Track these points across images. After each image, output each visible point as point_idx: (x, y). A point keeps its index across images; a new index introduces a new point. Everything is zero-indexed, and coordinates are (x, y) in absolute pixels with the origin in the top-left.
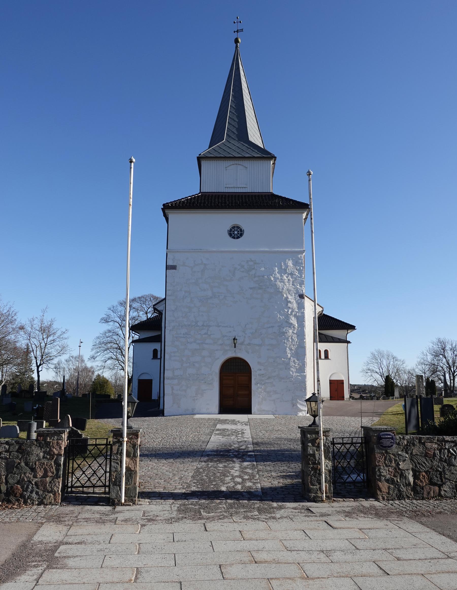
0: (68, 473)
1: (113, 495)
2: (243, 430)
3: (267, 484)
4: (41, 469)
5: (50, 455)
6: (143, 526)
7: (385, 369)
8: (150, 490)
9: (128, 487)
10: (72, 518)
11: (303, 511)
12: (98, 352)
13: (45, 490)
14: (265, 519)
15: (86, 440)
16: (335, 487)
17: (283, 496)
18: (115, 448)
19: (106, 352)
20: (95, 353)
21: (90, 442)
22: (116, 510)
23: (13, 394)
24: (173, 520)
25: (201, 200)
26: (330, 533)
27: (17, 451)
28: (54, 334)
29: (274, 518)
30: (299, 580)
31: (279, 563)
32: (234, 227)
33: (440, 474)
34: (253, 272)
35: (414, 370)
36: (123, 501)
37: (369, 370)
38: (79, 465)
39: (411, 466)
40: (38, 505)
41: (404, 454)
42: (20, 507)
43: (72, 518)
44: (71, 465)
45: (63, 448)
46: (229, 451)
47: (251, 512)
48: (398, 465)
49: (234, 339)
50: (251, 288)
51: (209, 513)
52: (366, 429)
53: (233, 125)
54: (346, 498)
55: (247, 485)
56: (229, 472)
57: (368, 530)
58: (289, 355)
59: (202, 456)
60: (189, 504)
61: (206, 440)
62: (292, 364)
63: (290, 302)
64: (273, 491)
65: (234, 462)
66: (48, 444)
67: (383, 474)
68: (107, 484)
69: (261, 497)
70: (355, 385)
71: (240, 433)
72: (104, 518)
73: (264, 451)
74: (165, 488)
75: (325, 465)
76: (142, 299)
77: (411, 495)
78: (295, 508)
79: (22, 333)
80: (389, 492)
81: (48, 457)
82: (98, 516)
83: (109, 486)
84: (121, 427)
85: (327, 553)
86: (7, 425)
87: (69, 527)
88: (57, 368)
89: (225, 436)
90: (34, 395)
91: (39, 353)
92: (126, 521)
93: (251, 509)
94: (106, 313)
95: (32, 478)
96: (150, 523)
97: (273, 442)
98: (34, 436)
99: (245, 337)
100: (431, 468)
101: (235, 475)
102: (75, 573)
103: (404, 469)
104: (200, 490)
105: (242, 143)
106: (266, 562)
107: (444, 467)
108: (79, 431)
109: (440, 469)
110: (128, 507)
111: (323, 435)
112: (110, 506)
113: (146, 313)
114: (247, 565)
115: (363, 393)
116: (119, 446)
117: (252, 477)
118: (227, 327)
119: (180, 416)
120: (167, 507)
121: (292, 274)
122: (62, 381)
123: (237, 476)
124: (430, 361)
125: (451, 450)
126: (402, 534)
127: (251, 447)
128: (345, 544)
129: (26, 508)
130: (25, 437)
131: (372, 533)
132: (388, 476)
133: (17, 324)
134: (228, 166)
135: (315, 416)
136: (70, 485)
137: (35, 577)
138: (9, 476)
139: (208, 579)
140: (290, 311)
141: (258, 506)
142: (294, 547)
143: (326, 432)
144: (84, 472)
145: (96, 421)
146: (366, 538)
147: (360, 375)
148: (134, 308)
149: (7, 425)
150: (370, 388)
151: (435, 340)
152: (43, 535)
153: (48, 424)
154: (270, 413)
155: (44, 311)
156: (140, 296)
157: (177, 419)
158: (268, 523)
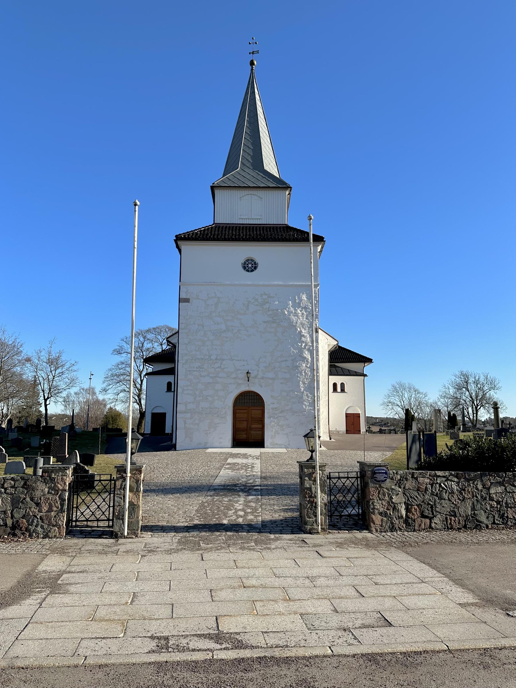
0: (73, 507)
1: (116, 529)
2: (253, 464)
3: (268, 517)
4: (45, 504)
5: (55, 490)
6: (142, 556)
7: (406, 402)
8: (153, 524)
9: (130, 520)
10: (75, 550)
11: (298, 542)
12: (110, 385)
13: (50, 524)
14: (261, 549)
15: (93, 476)
16: (331, 520)
17: (281, 528)
18: (118, 483)
19: (118, 384)
20: (107, 386)
21: (97, 478)
22: (119, 542)
23: (19, 428)
24: (173, 551)
25: (215, 232)
26: (320, 562)
27: (23, 487)
28: (63, 366)
29: (269, 549)
30: (281, 601)
31: (266, 587)
32: (248, 260)
33: (432, 507)
34: (267, 306)
35: (436, 403)
36: (126, 534)
37: (390, 402)
38: (83, 500)
39: (404, 500)
40: (43, 538)
41: (397, 488)
42: (25, 540)
43: (75, 550)
44: (75, 500)
45: (67, 484)
46: (235, 485)
47: (248, 543)
48: (391, 498)
49: (248, 373)
50: (265, 322)
51: (208, 544)
52: (362, 465)
53: (248, 153)
54: (340, 530)
55: (249, 518)
56: (233, 506)
57: (355, 559)
58: (302, 389)
59: (209, 490)
60: (190, 537)
61: (216, 474)
62: (305, 397)
63: (303, 336)
64: (272, 524)
65: (239, 496)
66: (52, 480)
67: (376, 507)
68: (111, 518)
69: (260, 529)
70: (377, 418)
71: (250, 467)
72: (106, 549)
73: (271, 485)
74: (168, 521)
75: (321, 498)
76: (157, 330)
77: (403, 527)
78: (290, 540)
79: (28, 365)
80: (382, 524)
81: (53, 492)
82: (100, 548)
83: (113, 520)
84: (125, 463)
85: (312, 579)
86: (12, 460)
87: (72, 558)
88: (66, 401)
89: (235, 470)
90: (41, 429)
91: (46, 386)
92: (127, 552)
93: (248, 540)
94: (118, 344)
95: (37, 513)
96: (150, 554)
97: (281, 476)
98: (40, 472)
99: (258, 371)
100: (423, 502)
101: (239, 509)
102: (76, 597)
103: (396, 502)
104: (203, 523)
105: (257, 172)
106: (254, 586)
107: (435, 501)
108: (86, 467)
109: (431, 503)
110: (130, 540)
111: (320, 470)
112: (113, 538)
113: (161, 345)
114: (237, 590)
115: (383, 426)
116: (122, 482)
117: (255, 510)
118: (240, 360)
119: (192, 450)
120: (168, 540)
121: (305, 308)
122: (72, 414)
123: (240, 510)
124: (452, 394)
125: (442, 484)
126: (386, 562)
127: (258, 482)
128: (330, 571)
129: (31, 541)
130: (32, 473)
131: (358, 562)
132: (381, 510)
133: (23, 356)
134: (243, 197)
135: (312, 451)
136: (74, 519)
137: (39, 601)
138: (15, 510)
139: (198, 601)
140: (303, 345)
141: (256, 537)
142: (282, 574)
143: (322, 467)
144: (88, 507)
145: (106, 456)
146: (351, 566)
147: (377, 408)
148: (148, 339)
149: (12, 460)
150: (392, 421)
151: (458, 373)
152: (47, 566)
153: (55, 459)
154: (283, 446)
155: (52, 342)
156: (155, 327)
157: (189, 453)
158: (263, 553)
